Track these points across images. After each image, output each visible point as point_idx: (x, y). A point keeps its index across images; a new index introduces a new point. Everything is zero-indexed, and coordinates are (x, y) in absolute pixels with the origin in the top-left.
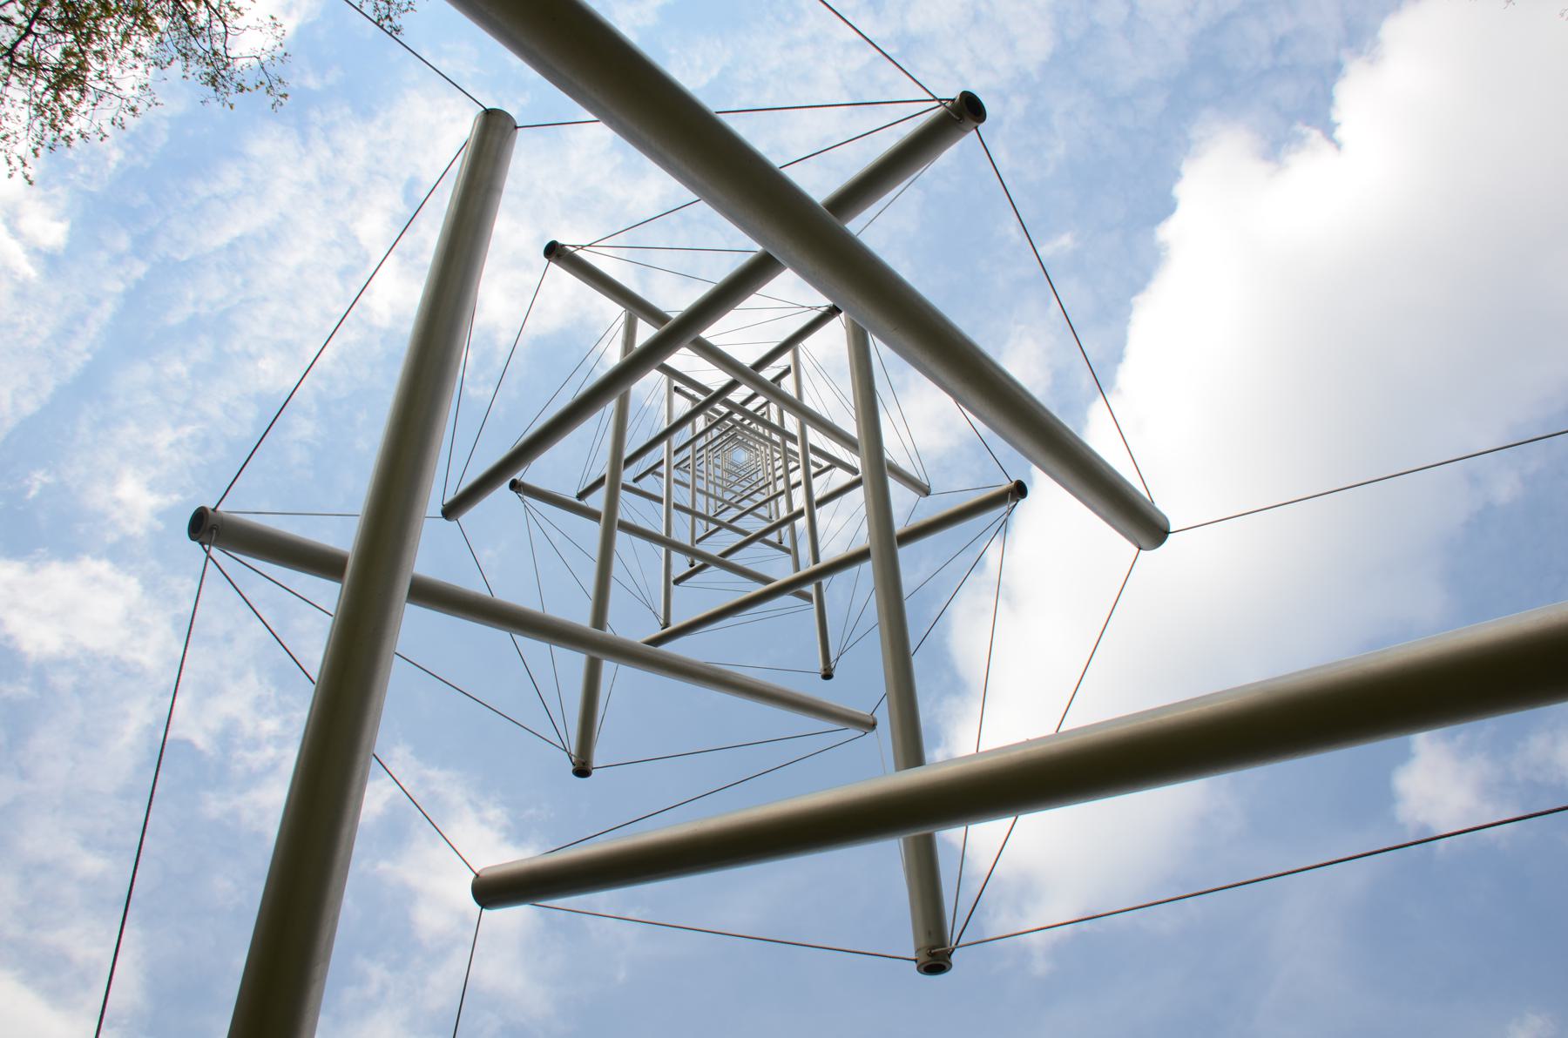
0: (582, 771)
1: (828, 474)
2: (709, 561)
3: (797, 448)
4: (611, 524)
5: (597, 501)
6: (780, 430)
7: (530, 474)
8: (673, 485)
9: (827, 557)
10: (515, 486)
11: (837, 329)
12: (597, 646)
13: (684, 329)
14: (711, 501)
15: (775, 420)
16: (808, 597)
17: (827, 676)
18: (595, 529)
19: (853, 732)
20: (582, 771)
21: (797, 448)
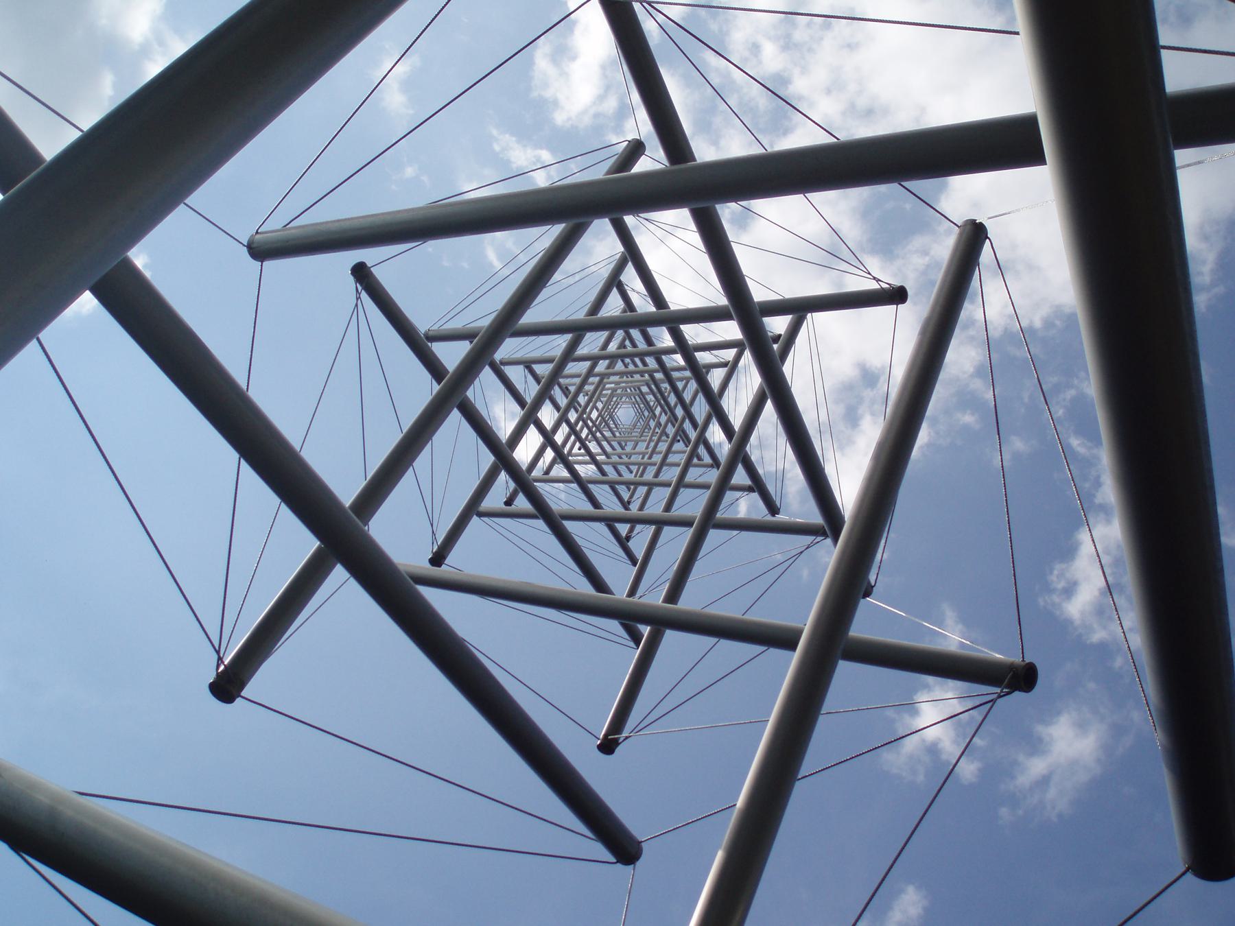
0: (227, 686)
1: (703, 469)
2: (542, 510)
3: (693, 435)
4: (452, 394)
5: (452, 355)
6: (687, 409)
7: (392, 265)
8: (444, 571)
9: (691, 601)
10: (361, 273)
11: (561, 380)
12: (341, 538)
13: (707, 191)
14: (577, 381)
15: (687, 396)
16: (636, 637)
17: (608, 746)
18: (424, 389)
19: (600, 851)
20: (227, 686)
21: (693, 435)
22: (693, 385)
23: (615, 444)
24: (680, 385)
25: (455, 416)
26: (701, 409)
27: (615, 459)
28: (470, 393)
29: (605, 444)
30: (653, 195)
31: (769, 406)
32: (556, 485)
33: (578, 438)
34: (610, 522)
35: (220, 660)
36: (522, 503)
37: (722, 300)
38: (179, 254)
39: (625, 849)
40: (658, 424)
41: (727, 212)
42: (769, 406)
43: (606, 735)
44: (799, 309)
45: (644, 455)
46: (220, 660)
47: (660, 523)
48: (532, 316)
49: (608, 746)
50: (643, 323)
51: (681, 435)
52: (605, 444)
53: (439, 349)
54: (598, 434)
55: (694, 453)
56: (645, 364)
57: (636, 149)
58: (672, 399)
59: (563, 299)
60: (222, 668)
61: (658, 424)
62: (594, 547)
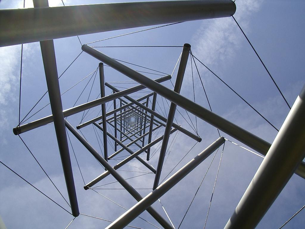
0: (17, 131)
4: (102, 102)
7: (107, 68)
17: (86, 188)
19: (70, 210)
20: (17, 131)
22: (149, 124)
23: (127, 124)
24: (147, 122)
25: (100, 106)
26: (147, 130)
27: (125, 127)
28: (106, 104)
29: (125, 123)
30: (166, 93)
31: (162, 141)
32: (111, 126)
33: (121, 119)
34: (116, 141)
35: (19, 125)
36: (101, 126)
37: (167, 118)
38: (65, 47)
39: (75, 212)
40: (138, 126)
41: (178, 108)
42: (162, 141)
43: (87, 186)
44: (178, 128)
45: (131, 130)
46: (19, 125)
47: (124, 148)
48: (129, 95)
49: (86, 188)
50: (148, 110)
51: (141, 132)
52: (125, 123)
53: (106, 88)
54: (125, 120)
55: (141, 138)
56: (143, 111)
57: (169, 78)
58: (143, 123)
59: (136, 96)
60: (18, 127)
61: (138, 126)
62: (110, 142)
